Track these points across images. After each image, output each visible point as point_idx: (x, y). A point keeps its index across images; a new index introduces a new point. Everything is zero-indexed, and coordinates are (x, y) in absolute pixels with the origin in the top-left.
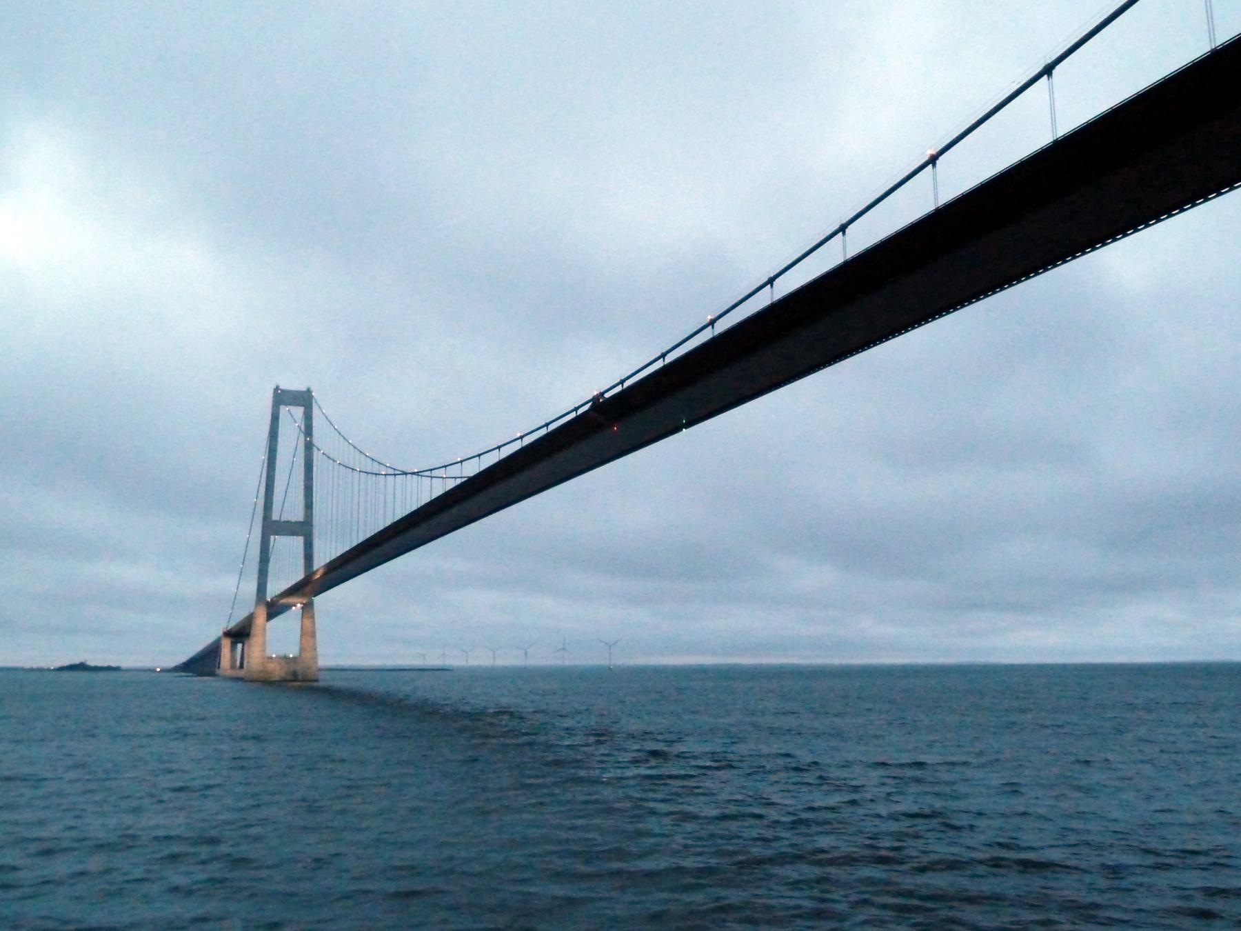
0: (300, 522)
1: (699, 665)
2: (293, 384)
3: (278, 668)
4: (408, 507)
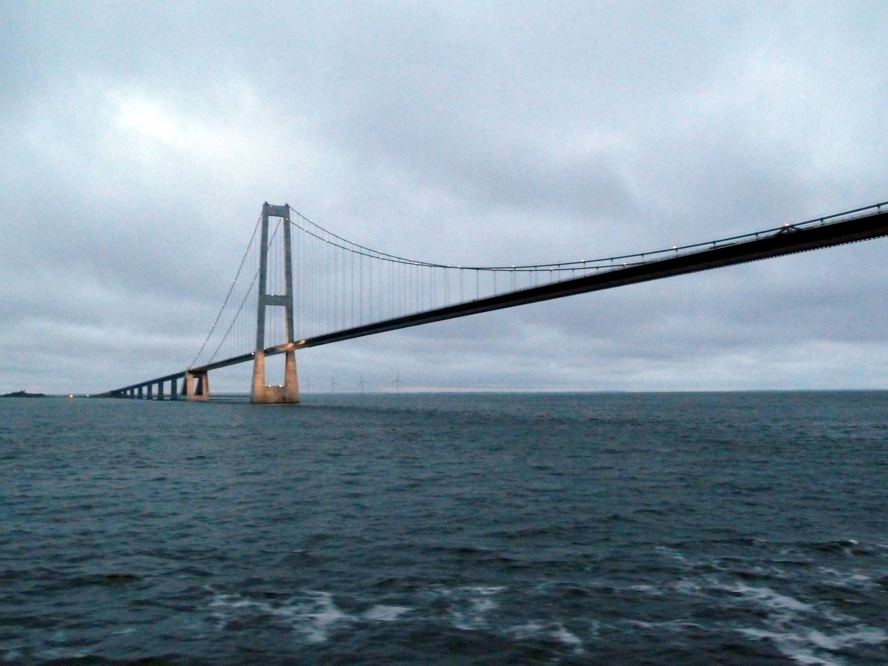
0: (283, 296)
1: (419, 393)
2: (277, 201)
3: (274, 394)
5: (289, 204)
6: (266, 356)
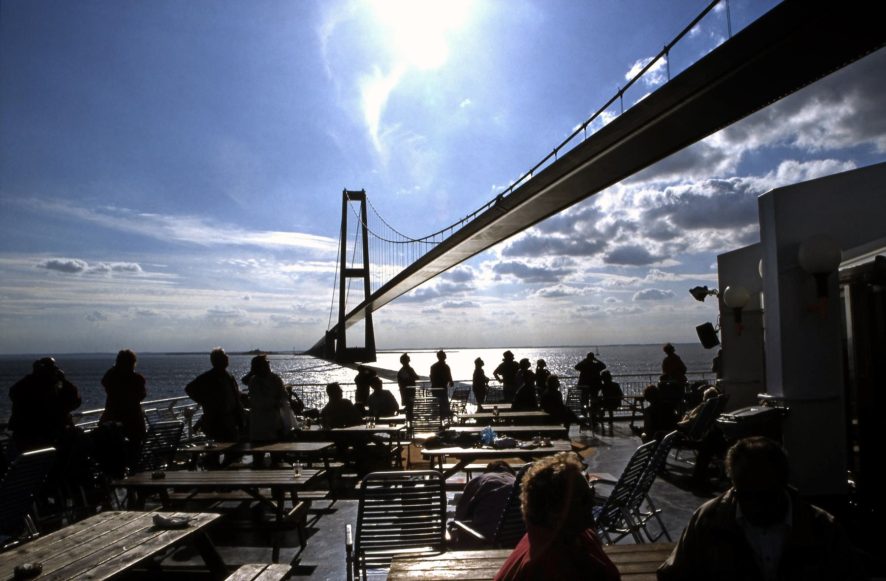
4: (381, 283)
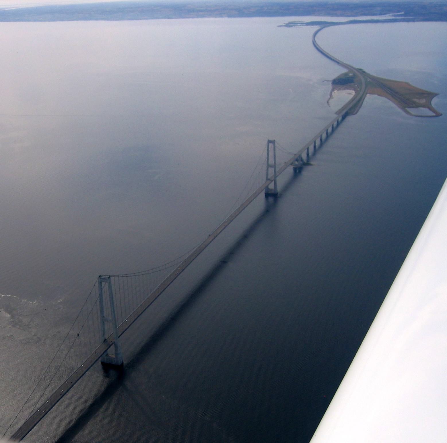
2: (271, 139)
5: (275, 140)
6: (294, 168)
